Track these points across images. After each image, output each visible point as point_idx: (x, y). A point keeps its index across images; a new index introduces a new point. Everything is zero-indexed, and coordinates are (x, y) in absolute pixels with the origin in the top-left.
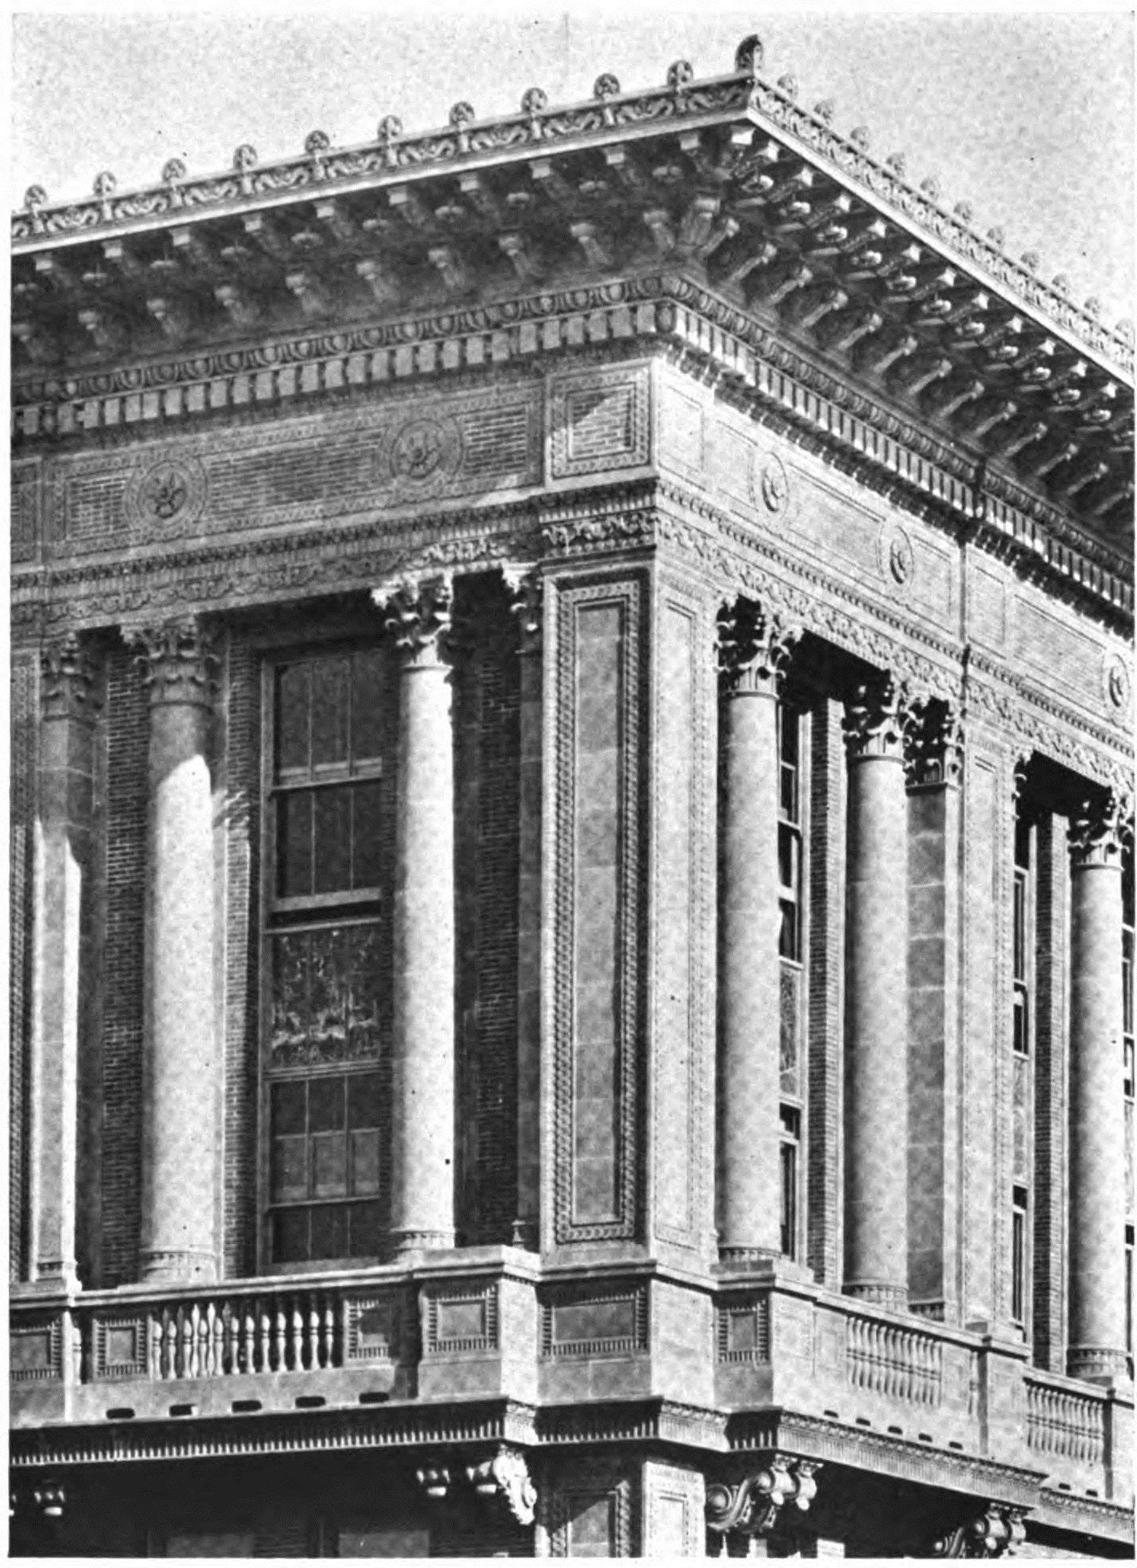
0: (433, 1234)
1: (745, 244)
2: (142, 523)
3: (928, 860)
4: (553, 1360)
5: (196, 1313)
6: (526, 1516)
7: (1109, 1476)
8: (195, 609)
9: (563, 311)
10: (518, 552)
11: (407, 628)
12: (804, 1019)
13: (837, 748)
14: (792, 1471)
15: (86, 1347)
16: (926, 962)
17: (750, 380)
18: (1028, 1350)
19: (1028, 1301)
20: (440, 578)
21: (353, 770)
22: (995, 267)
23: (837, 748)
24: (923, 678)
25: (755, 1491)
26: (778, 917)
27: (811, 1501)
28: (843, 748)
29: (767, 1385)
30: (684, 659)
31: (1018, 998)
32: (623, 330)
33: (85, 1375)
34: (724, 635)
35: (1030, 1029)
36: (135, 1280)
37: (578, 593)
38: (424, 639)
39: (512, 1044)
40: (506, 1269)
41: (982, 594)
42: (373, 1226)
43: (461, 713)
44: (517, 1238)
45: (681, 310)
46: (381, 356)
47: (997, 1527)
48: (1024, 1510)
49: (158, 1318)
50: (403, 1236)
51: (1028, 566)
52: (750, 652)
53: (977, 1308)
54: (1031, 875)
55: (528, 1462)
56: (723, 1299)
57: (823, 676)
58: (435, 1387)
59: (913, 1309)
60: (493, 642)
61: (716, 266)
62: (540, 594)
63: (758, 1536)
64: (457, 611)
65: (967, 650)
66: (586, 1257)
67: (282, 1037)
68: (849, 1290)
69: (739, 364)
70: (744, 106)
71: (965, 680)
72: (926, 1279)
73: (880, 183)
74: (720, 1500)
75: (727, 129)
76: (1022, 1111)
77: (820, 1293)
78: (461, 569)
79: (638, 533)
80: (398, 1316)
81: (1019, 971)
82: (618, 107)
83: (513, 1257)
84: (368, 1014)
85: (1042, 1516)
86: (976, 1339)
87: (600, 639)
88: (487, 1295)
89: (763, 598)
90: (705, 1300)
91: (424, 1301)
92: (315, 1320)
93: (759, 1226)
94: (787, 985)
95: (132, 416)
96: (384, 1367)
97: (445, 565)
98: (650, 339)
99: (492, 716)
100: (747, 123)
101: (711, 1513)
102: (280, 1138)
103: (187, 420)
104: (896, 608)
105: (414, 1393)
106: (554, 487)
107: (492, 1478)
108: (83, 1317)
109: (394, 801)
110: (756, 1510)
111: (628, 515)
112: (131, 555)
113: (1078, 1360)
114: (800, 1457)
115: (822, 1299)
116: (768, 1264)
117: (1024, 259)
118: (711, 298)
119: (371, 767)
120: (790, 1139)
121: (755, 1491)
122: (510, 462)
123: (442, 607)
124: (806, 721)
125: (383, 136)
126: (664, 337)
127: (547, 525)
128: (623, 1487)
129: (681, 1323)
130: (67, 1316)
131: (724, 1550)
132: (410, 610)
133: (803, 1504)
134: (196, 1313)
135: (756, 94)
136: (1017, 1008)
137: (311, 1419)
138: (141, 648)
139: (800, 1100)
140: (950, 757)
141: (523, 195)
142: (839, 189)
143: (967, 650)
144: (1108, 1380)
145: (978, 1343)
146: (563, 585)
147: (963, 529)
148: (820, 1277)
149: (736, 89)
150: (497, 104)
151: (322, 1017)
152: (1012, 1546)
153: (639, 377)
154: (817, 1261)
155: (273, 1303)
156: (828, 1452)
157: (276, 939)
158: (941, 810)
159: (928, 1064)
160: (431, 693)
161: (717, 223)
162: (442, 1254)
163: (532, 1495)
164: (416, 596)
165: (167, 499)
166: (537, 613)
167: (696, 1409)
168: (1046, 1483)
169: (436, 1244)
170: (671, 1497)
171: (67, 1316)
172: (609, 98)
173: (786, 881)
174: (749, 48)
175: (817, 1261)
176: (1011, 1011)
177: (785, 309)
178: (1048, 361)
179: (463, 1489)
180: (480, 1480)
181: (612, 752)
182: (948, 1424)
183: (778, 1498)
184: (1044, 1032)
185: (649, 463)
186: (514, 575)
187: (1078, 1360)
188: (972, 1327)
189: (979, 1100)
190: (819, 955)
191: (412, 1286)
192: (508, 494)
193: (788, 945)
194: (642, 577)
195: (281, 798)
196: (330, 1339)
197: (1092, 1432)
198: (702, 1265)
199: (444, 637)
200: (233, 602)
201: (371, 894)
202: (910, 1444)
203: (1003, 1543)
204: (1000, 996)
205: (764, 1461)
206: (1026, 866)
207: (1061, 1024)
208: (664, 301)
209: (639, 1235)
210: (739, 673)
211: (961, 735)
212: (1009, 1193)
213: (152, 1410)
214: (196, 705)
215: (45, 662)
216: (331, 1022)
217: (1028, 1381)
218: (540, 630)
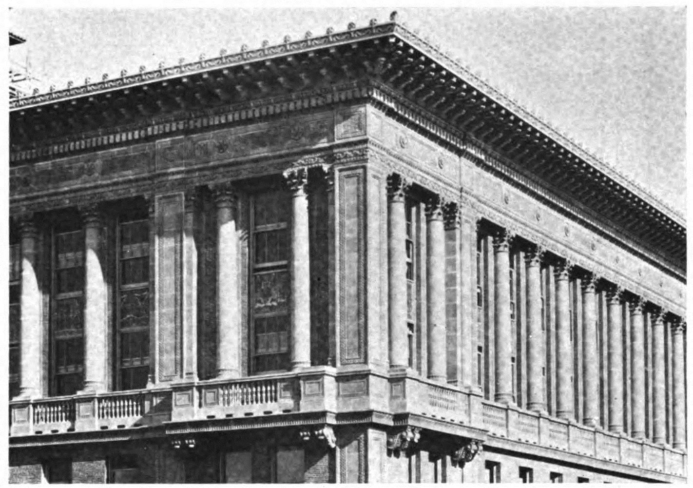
0: (303, 363)
1: (393, 71)
2: (216, 154)
3: (450, 251)
4: (341, 399)
5: (233, 387)
6: (333, 445)
7: (508, 431)
8: (230, 179)
9: (340, 90)
10: (326, 161)
11: (294, 184)
12: (414, 296)
13: (552, 279)
14: (413, 431)
15: (200, 398)
16: (451, 280)
17: (396, 110)
18: (483, 394)
19: (483, 381)
20: (303, 170)
21: (278, 226)
22: (416, 41)
23: (552, 279)
24: (448, 196)
25: (401, 437)
26: (406, 267)
27: (419, 440)
28: (425, 217)
29: (404, 406)
30: (377, 191)
31: (479, 291)
32: (358, 95)
33: (200, 405)
34: (389, 184)
35: (482, 300)
36: (215, 377)
37: (345, 173)
38: (299, 187)
39: (327, 305)
40: (326, 373)
41: (464, 169)
42: (286, 360)
43: (310, 209)
44: (329, 363)
45: (375, 91)
46: (285, 105)
47: (474, 447)
48: (482, 441)
49: (222, 389)
50: (295, 363)
51: (479, 162)
52: (397, 189)
53: (468, 382)
54: (482, 254)
55: (334, 429)
56: (391, 380)
57: (419, 196)
58: (306, 407)
59: (448, 382)
60: (319, 187)
61: (385, 78)
62: (333, 174)
63: (403, 450)
64: (309, 179)
65: (462, 188)
66: (351, 369)
67: (258, 305)
68: (429, 377)
69: (392, 105)
70: (392, 31)
71: (461, 197)
72: (452, 374)
73: (434, 52)
74: (391, 440)
75: (387, 38)
76: (480, 324)
77: (420, 378)
78: (310, 166)
79: (363, 155)
80: (294, 386)
81: (478, 282)
82: (355, 32)
83: (329, 369)
84: (284, 298)
85: (487, 443)
86: (467, 391)
87: (350, 187)
88: (320, 380)
89: (400, 173)
90: (386, 380)
91: (301, 382)
92: (269, 388)
93: (401, 359)
94: (409, 287)
95: (211, 123)
96: (289, 403)
97: (304, 165)
98: (366, 98)
99: (319, 209)
100: (393, 36)
101: (389, 443)
102: (259, 335)
103: (228, 125)
104: (589, 262)
105: (299, 410)
106: (337, 142)
107: (323, 434)
108: (199, 388)
109: (290, 235)
110: (466, 455)
111: (360, 150)
112: (211, 164)
113: (497, 397)
114: (415, 427)
115: (421, 380)
116: (404, 370)
117: (436, 46)
118: (384, 86)
119: (283, 225)
120: (411, 333)
121: (401, 437)
122: (325, 135)
123: (304, 178)
124: (414, 210)
125: (285, 41)
126: (369, 99)
127: (336, 153)
128: (362, 436)
129: (378, 386)
130: (195, 389)
131: (393, 455)
132: (295, 178)
133: (416, 440)
134: (233, 387)
135: (396, 27)
136: (478, 294)
137: (268, 417)
138: (214, 191)
139: (414, 321)
140: (457, 219)
141: (327, 57)
142: (422, 54)
143: (462, 188)
144: (619, 433)
145: (468, 392)
146: (340, 171)
147: (460, 153)
148: (420, 374)
149: (390, 27)
150: (319, 31)
151: (270, 299)
152: (479, 452)
153: (362, 109)
154: (419, 369)
155: (256, 384)
156: (423, 425)
157: (255, 276)
158: (455, 235)
159: (451, 310)
160: (301, 203)
161: (385, 65)
162: (307, 368)
163: (335, 439)
164: (296, 174)
165: (222, 148)
166: (333, 179)
167: (383, 413)
168: (489, 433)
169: (305, 366)
170: (376, 440)
171: (195, 389)
172: (352, 29)
173: (409, 256)
174: (394, 14)
175: (419, 369)
176: (476, 295)
177: (406, 90)
178: (464, 90)
179: (313, 436)
180: (319, 435)
181: (356, 219)
182: (458, 416)
183: (409, 439)
184: (486, 301)
185: (366, 134)
186: (326, 168)
187: (497, 397)
188: (466, 388)
189: (468, 321)
190: (418, 277)
191: (298, 378)
192: (323, 143)
193: (409, 275)
194: (365, 168)
195: (258, 235)
196: (273, 394)
197: (502, 419)
198: (384, 371)
199: (305, 186)
200: (241, 177)
201: (284, 262)
202: (448, 423)
203: (476, 452)
204: (472, 290)
205: (404, 428)
206: (480, 251)
207: (491, 298)
208: (370, 88)
209: (366, 362)
210: (393, 196)
211: (460, 213)
212: (476, 348)
213: (220, 416)
214: (231, 207)
215: (186, 196)
216: (273, 300)
217: (483, 403)
218: (333, 184)
